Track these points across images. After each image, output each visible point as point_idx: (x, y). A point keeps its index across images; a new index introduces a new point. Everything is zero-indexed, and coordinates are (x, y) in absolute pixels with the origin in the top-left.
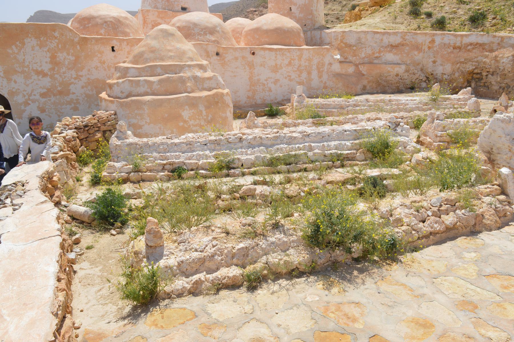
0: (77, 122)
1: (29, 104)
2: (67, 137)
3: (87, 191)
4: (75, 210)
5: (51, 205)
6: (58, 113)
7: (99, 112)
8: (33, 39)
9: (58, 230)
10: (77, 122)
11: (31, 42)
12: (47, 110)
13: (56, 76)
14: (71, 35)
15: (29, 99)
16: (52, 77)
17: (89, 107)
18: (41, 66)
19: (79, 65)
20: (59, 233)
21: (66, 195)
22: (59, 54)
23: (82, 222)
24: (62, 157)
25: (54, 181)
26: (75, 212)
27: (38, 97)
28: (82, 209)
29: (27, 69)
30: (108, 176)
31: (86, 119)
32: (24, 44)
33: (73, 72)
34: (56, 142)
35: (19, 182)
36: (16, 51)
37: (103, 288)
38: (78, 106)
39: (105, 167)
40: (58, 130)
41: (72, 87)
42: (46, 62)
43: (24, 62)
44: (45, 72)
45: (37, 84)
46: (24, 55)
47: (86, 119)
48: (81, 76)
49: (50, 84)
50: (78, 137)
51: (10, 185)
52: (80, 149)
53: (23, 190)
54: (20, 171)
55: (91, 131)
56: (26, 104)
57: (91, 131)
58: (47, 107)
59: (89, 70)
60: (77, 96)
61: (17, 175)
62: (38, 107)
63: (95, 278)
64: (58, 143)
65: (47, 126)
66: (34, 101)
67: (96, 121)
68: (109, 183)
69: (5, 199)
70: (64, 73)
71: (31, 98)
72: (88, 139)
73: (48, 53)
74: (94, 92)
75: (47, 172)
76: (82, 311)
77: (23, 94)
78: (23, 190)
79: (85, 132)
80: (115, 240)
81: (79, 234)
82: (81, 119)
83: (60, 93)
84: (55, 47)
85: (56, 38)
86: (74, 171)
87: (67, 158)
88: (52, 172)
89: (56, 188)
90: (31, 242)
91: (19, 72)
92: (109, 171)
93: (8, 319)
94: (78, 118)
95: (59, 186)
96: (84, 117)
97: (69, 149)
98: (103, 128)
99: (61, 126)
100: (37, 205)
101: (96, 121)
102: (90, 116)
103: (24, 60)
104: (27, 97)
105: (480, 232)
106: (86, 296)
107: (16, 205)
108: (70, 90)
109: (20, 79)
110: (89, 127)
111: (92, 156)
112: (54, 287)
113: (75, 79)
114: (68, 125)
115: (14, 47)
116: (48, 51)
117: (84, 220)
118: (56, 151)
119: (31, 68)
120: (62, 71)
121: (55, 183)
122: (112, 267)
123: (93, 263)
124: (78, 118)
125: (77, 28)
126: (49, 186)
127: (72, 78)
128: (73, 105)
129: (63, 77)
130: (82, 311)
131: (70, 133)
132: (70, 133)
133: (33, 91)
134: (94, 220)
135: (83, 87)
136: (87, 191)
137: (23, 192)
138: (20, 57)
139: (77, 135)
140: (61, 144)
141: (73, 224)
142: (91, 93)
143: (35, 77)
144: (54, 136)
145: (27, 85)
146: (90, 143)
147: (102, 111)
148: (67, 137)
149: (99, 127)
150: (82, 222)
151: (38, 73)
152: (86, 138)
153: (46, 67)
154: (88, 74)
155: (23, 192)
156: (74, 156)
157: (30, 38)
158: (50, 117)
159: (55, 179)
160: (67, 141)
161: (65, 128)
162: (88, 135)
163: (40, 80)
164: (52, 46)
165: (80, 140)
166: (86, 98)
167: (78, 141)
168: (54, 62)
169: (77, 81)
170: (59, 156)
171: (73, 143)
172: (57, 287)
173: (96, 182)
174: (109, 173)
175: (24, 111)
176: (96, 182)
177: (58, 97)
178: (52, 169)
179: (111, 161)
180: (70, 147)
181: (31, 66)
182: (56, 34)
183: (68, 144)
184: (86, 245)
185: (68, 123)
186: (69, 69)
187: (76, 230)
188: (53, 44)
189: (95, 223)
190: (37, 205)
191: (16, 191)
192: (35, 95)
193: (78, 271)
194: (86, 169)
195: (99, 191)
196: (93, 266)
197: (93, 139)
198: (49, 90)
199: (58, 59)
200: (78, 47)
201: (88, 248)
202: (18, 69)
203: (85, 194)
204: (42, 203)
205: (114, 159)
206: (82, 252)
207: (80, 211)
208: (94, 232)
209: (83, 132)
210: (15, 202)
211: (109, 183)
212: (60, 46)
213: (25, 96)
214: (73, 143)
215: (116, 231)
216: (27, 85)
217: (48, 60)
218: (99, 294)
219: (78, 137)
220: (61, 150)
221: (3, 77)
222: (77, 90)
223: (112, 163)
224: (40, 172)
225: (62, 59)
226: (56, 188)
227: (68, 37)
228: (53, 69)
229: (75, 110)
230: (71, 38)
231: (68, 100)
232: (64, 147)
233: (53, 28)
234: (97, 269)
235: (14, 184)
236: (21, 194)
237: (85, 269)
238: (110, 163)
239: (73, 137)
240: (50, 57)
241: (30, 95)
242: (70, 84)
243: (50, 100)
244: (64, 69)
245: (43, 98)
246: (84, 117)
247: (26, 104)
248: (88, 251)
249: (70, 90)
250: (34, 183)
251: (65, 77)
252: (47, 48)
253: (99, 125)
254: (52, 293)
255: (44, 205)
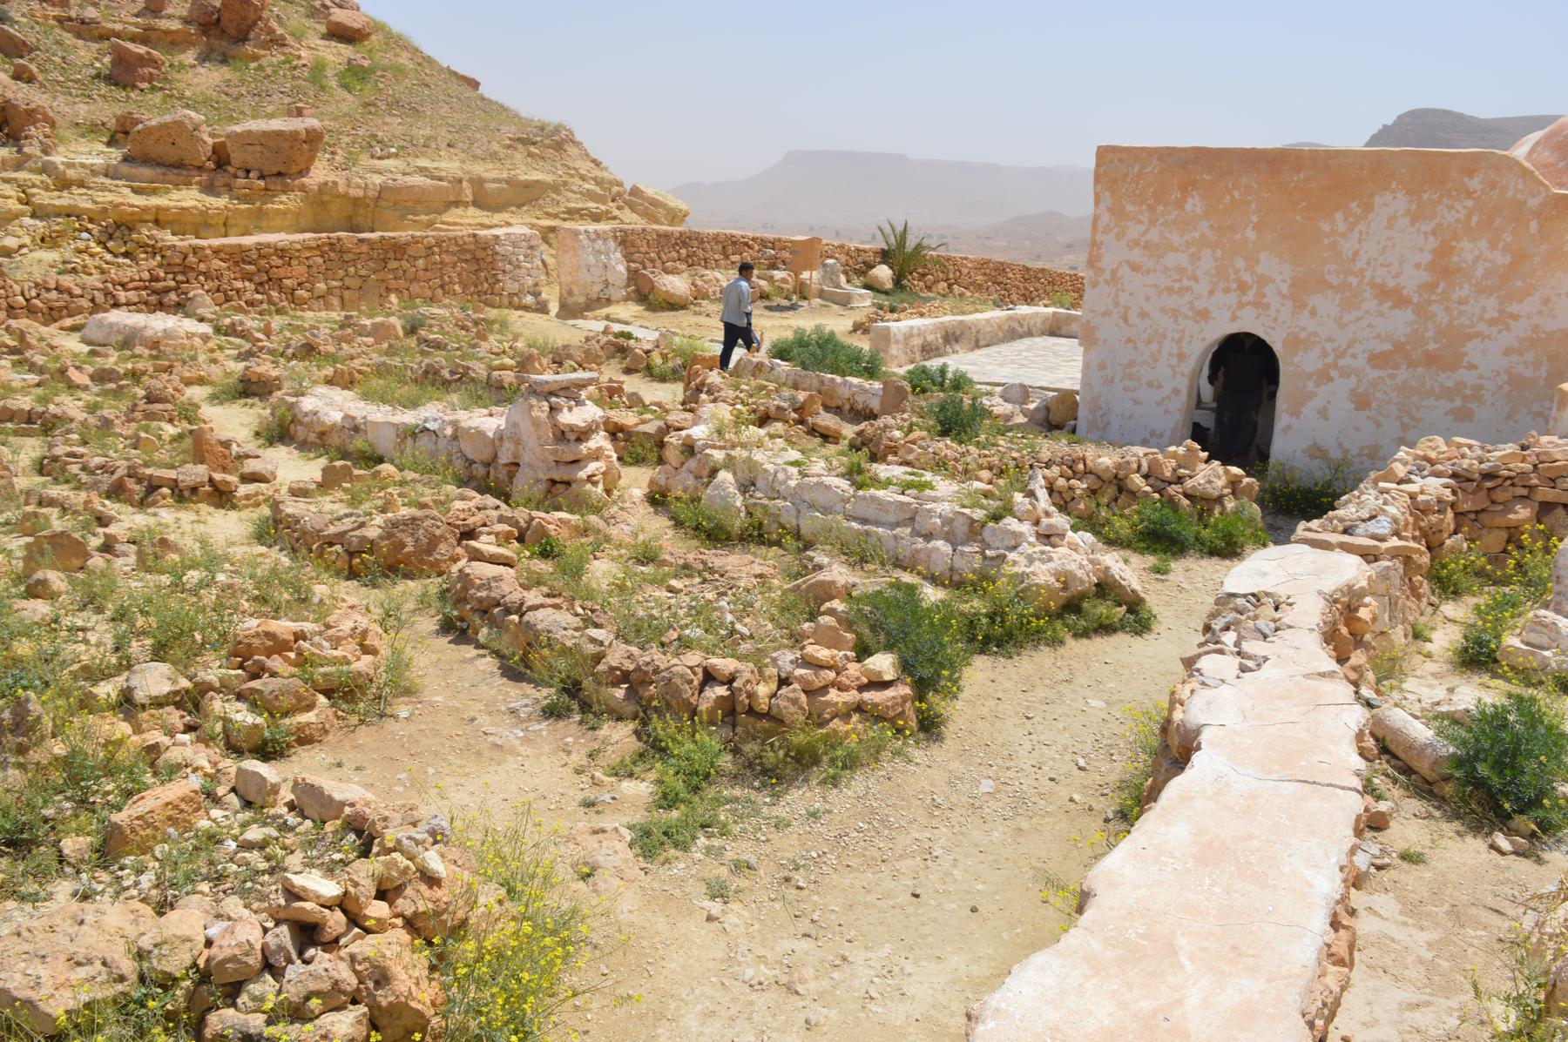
0: (1463, 456)
1: (1331, 379)
2: (1421, 498)
3: (1435, 675)
4: (1398, 724)
5: (1344, 691)
6: (1406, 420)
7: (1544, 439)
8: (1399, 195)
9: (1358, 774)
10: (1463, 456)
11: (1391, 203)
12: (1374, 405)
13: (1434, 308)
14: (1520, 186)
15: (1335, 366)
16: (1422, 311)
17: (1509, 417)
18: (1397, 276)
19: (1519, 283)
20: (1357, 783)
21: (1375, 667)
22: (1465, 244)
23: (1407, 770)
24: (1394, 554)
25: (1359, 619)
26: (1396, 732)
27: (1361, 362)
28: (1421, 732)
29: (1353, 281)
30: (1524, 652)
31: (1497, 454)
32: (1368, 208)
33: (1491, 305)
34: (1385, 503)
35: (1267, 594)
36: (1341, 226)
37: (1428, 1004)
38: (1473, 406)
39: (1521, 622)
40: (1400, 470)
41: (1473, 351)
42: (1418, 266)
43: (1354, 261)
44: (1405, 292)
45: (1370, 325)
46: (1360, 241)
47: (1497, 454)
48: (1515, 317)
49: (1408, 330)
50: (1453, 505)
51: (1245, 596)
52: (1448, 542)
53: (1275, 621)
54: (1275, 564)
55: (1500, 496)
56: (1324, 377)
57: (1500, 496)
58: (1377, 394)
59: (1546, 301)
60: (1481, 377)
61: (1265, 574)
62: (1353, 392)
63: (1410, 959)
64: (1391, 510)
65: (1362, 449)
66: (1345, 373)
67: (1528, 467)
68: (1526, 676)
69: (1222, 630)
70: (1461, 302)
71: (1341, 362)
72: (1482, 516)
73: (1431, 239)
74: (1543, 372)
75: (1350, 587)
76: (974, 910)
77: (1324, 349)
78: (1275, 621)
79: (1481, 494)
80: (1502, 870)
81: (1389, 803)
82: (1479, 452)
83: (1431, 360)
84: (1458, 220)
85: (1469, 195)
86: (1412, 604)
87: (1407, 561)
88: (1362, 593)
89: (1359, 642)
90: (1275, 777)
91: (1331, 287)
92: (1533, 637)
93: (1189, 967)
94: (1470, 447)
95: (1368, 637)
96: (1489, 447)
97: (1417, 533)
98: (1546, 493)
99: (1410, 458)
100: (1306, 676)
101: (1528, 467)
102: (1510, 448)
103: (1356, 254)
104: (1330, 359)
105: (38, 597)
106: (1369, 1004)
107: (1249, 658)
108: (1465, 354)
109: (1328, 305)
110: (1499, 481)
111: (1480, 573)
112: (1320, 941)
113: (1492, 322)
114: (1432, 462)
115: (1339, 216)
116: (1433, 232)
117: (1415, 764)
118: (1381, 531)
119: (1367, 279)
120: (1455, 297)
121: (1359, 625)
122: (1470, 950)
123: (1413, 910)
124: (1470, 447)
125: (1547, 166)
126: (1345, 632)
127: (1481, 319)
128: (1458, 403)
129: (1455, 313)
130: (974, 910)
131: (1433, 487)
132: (1433, 487)
133: (1350, 345)
134: (1447, 779)
135: (1508, 352)
136: (1435, 675)
137: (1272, 625)
138: (1348, 247)
139: (1452, 498)
140: (1399, 515)
141: (1377, 765)
142: (1528, 373)
143: (1371, 304)
144: (1381, 484)
145: (1342, 327)
146: (1484, 532)
147: (1555, 439)
148: (1421, 498)
149: (1531, 488)
150: (1407, 770)
151: (1383, 293)
152: (1477, 512)
153: (1411, 280)
154: (1540, 313)
155: (1272, 625)
156: (1425, 559)
157: (1393, 192)
158: (1378, 424)
159: (1363, 613)
160: (1419, 509)
161: (1421, 469)
162: (1486, 504)
163: (1382, 315)
164: (1451, 217)
165: (1456, 514)
166: (1506, 388)
167: (1450, 514)
168: (1443, 267)
169: (1494, 330)
170: (1388, 550)
171: (1434, 518)
172: (1329, 946)
173: (1477, 657)
174: (1528, 644)
175: (1311, 396)
176: (1477, 657)
177: (1420, 370)
178: (1364, 583)
179: (1546, 606)
180: (1420, 529)
181: (1368, 275)
182: (1475, 184)
183: (1417, 519)
184: (1400, 845)
185: (1433, 455)
186: (1481, 291)
187: (1383, 787)
188: (1453, 213)
189: (1448, 789)
190: (1306, 676)
191: (1256, 618)
192: (1354, 356)
193: (1362, 912)
194: (1449, 609)
195: (1474, 694)
196: (1410, 921)
197: (1499, 521)
198: (1399, 347)
199: (1455, 259)
200: (1534, 226)
201: (1406, 857)
202: (1333, 280)
203: (1430, 686)
204: (1322, 675)
205: (1559, 603)
206: (1387, 860)
207: (1413, 734)
208: (1437, 814)
209: (1474, 492)
210: (1247, 646)
211: (1526, 676)
212: (1475, 219)
213: (1325, 355)
214: (1434, 518)
215: (1512, 842)
216: (1342, 327)
217: (1426, 258)
218: (1408, 1014)
219: (1453, 505)
220: (1397, 533)
221: (1284, 297)
222: (1488, 358)
223: (1549, 615)
224: (1331, 584)
225: (1469, 257)
226: (1359, 642)
227: (1510, 194)
228: (1431, 287)
229: (1462, 419)
230: (1520, 196)
231: (1449, 384)
232: (1407, 524)
233: (1470, 165)
234: (1423, 937)
235: (1253, 595)
236: (1266, 631)
237: (1380, 916)
238: (1542, 612)
239: (1440, 501)
240: (1434, 252)
241: (1342, 355)
242: (1471, 337)
243: (1392, 377)
244: (1466, 290)
245: (1375, 366)
246: (1489, 447)
247: (1324, 377)
248: (1405, 865)
249: (1465, 354)
250: (1309, 613)
251: (1461, 314)
252: (1433, 224)
253: (1535, 481)
254: (1314, 956)
255: (1326, 685)
